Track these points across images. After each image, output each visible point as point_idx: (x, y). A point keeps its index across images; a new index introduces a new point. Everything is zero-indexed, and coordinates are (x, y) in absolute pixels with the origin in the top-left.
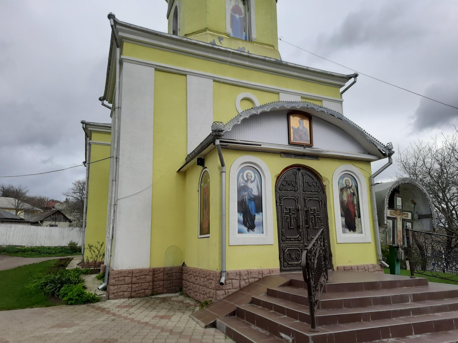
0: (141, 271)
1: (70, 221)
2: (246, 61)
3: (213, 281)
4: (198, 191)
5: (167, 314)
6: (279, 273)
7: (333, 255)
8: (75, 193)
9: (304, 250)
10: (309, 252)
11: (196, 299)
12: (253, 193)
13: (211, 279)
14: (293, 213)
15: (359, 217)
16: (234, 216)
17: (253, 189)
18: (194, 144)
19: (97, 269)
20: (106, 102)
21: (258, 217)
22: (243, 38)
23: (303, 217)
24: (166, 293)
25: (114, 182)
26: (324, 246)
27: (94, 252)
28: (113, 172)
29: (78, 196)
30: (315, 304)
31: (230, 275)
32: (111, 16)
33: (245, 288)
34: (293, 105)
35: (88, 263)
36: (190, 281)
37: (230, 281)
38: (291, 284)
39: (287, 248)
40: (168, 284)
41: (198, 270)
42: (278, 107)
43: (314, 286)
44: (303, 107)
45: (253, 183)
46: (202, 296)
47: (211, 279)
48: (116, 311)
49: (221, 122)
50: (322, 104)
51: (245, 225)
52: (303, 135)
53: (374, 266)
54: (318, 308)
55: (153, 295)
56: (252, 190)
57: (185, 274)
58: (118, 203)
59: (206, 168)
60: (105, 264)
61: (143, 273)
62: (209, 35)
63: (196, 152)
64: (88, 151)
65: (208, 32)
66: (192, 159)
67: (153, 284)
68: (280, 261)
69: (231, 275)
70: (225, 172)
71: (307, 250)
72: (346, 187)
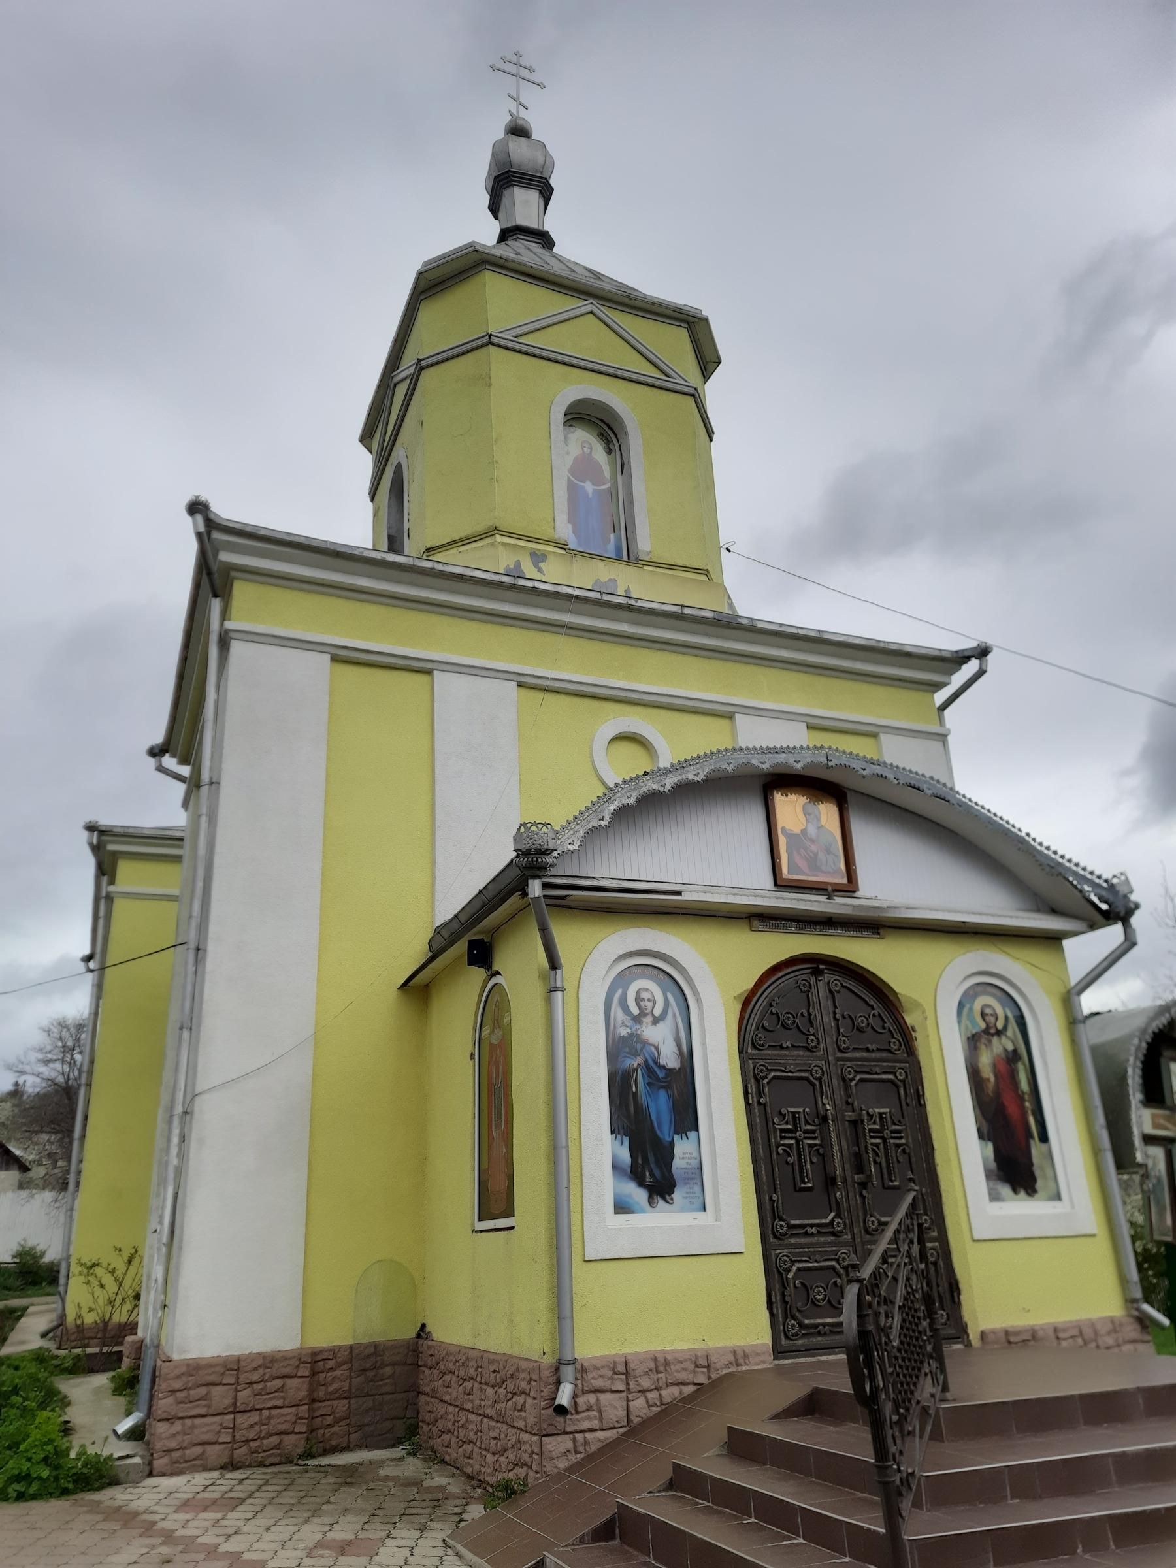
0: (268, 1361)
1: (24, 1168)
2: (619, 620)
3: (529, 1401)
4: (472, 1055)
5: (362, 1535)
6: (767, 1361)
7: (962, 1286)
8: (46, 1062)
9: (850, 1281)
10: (871, 1286)
11: (469, 1470)
12: (662, 1062)
13: (523, 1392)
14: (806, 1132)
15: (1044, 1138)
16: (598, 1146)
17: (661, 1047)
18: (455, 894)
19: (112, 1351)
20: (169, 762)
21: (683, 1149)
22: (610, 550)
23: (844, 1143)
24: (360, 1447)
25: (186, 1033)
26: (923, 1256)
27: (102, 1286)
28: (183, 999)
29: (53, 1075)
30: (904, 1490)
31: (590, 1375)
32: (197, 508)
33: (646, 1422)
34: (781, 758)
35: (80, 1328)
36: (447, 1398)
37: (592, 1398)
38: (814, 1405)
39: (793, 1262)
40: (366, 1408)
41: (472, 1354)
42: (730, 768)
43: (895, 1418)
44: (812, 765)
45: (661, 1025)
46: (490, 1458)
47: (523, 1392)
48: (174, 1521)
49: (544, 824)
50: (879, 748)
51: (641, 1183)
52: (821, 856)
53: (1114, 1326)
54: (917, 1504)
55: (312, 1456)
56: (657, 1048)
57: (427, 1372)
58: (196, 1108)
59: (498, 973)
60: (140, 1333)
61: (274, 1371)
62: (501, 548)
63: (463, 918)
64: (101, 922)
65: (498, 538)
66: (451, 943)
67: (311, 1410)
68: (772, 1316)
69: (595, 1374)
70: (563, 989)
71: (859, 1281)
72: (986, 1031)
